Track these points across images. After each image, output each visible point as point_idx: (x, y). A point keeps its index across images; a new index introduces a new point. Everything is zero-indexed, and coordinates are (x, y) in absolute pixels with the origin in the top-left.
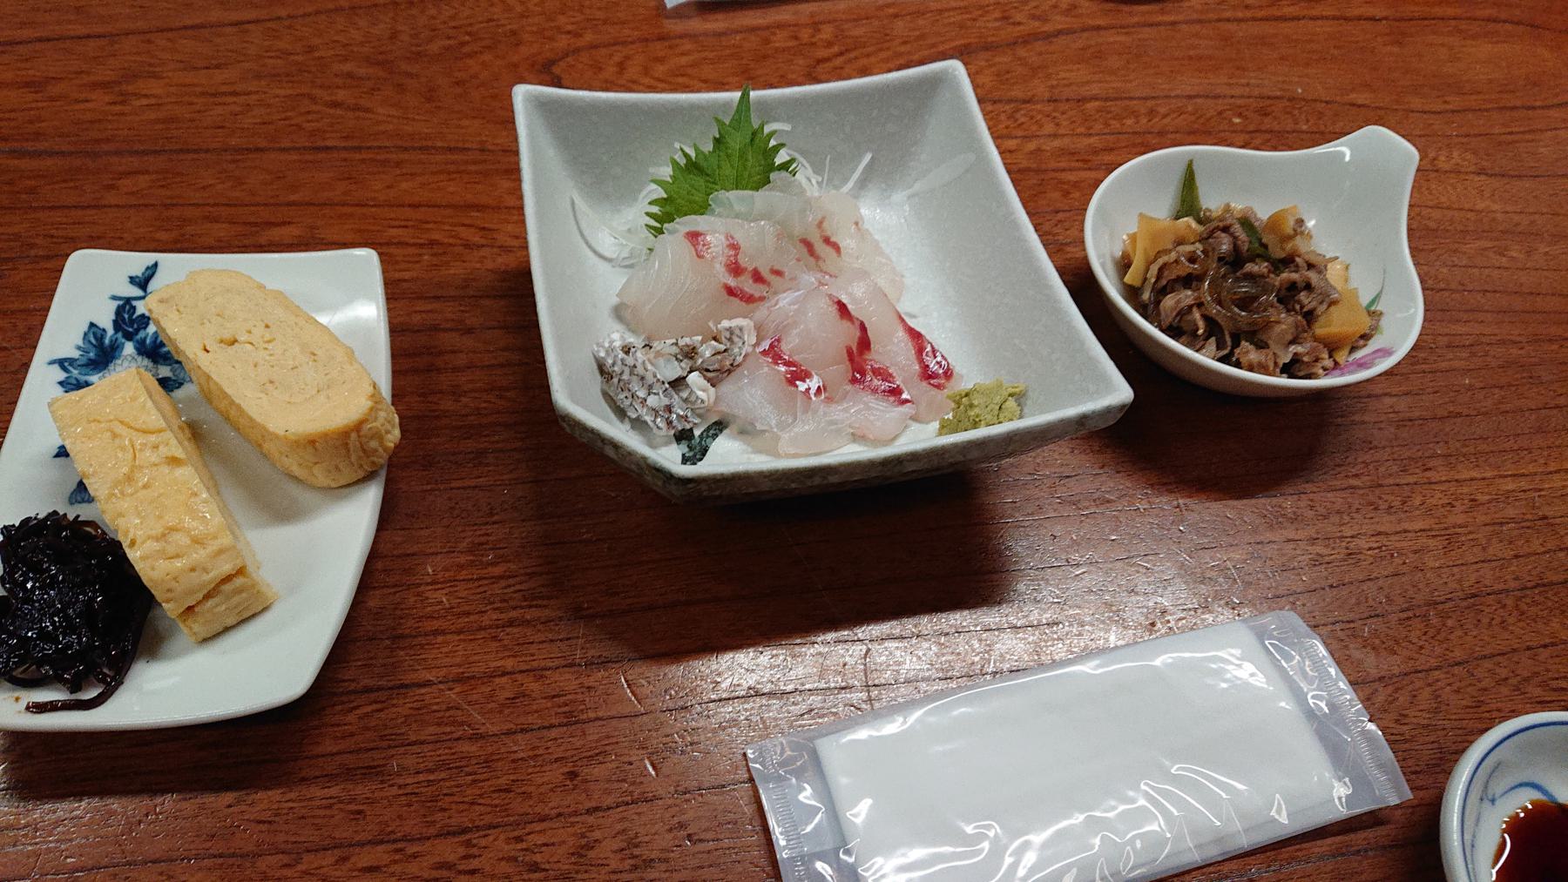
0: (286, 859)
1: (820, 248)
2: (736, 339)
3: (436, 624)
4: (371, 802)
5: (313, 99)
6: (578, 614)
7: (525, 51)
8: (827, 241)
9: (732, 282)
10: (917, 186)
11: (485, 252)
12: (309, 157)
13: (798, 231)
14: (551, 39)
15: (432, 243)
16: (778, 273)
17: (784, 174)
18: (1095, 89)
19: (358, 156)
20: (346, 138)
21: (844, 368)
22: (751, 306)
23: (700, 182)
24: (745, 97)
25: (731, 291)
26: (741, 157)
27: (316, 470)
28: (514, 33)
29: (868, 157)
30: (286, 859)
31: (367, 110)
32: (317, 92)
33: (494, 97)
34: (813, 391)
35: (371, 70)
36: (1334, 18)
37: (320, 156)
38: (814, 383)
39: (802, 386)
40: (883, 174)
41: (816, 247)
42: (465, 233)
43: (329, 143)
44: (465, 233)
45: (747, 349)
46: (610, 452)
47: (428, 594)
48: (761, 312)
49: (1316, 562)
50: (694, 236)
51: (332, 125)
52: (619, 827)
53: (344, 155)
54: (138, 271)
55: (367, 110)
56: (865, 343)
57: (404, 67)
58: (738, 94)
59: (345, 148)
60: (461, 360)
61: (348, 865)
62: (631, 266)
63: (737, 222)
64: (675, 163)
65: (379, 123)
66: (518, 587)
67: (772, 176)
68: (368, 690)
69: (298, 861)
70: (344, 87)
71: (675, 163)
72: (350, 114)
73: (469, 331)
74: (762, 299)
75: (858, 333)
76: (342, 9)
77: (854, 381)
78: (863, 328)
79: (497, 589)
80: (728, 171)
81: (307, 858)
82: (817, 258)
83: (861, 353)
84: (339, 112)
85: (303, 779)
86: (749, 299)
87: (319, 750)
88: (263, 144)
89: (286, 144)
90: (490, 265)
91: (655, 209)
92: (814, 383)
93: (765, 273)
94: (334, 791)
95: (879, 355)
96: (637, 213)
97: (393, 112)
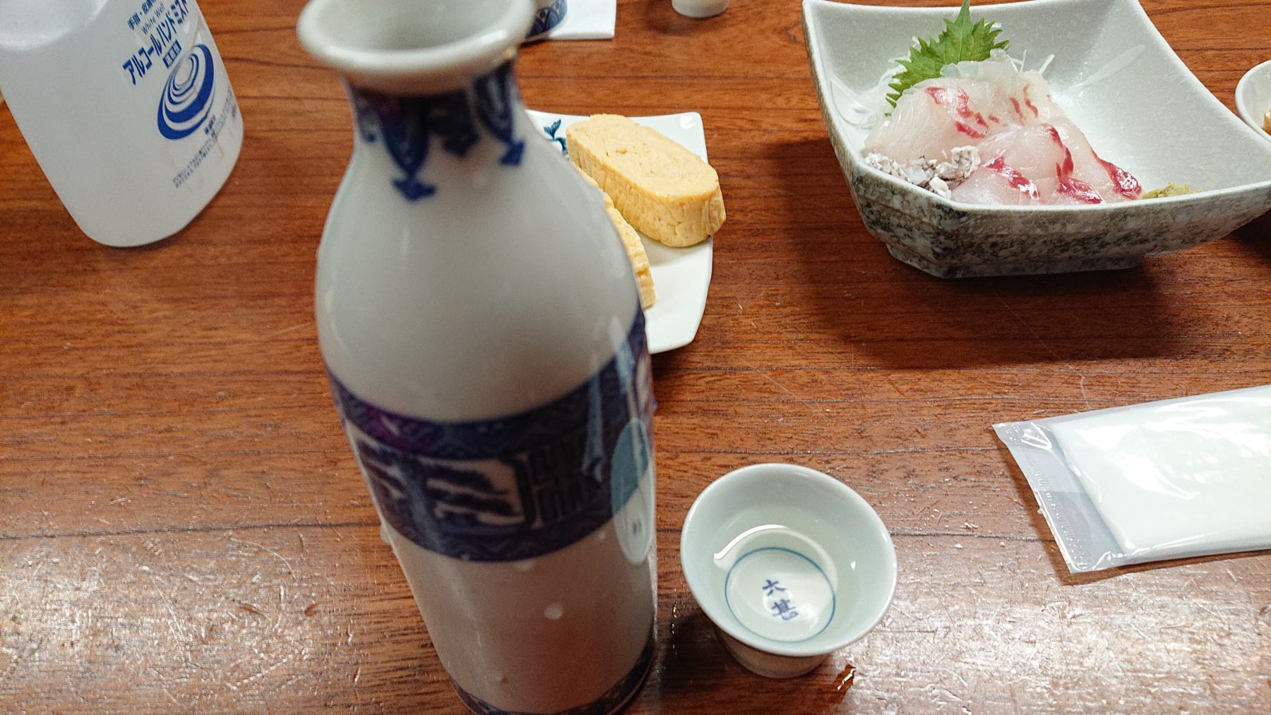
0: (668, 455)
1: (1023, 107)
2: (964, 161)
3: (749, 337)
4: (721, 429)
5: (631, 50)
6: (847, 339)
7: (767, 22)
8: (1028, 103)
9: (962, 120)
10: (1091, 79)
11: (753, 133)
13: (1009, 92)
14: (786, 15)
15: (718, 128)
16: (995, 119)
17: (1000, 51)
18: (1210, 44)
21: (1051, 181)
22: (976, 140)
23: (932, 62)
24: (965, 13)
25: (961, 128)
26: (964, 43)
27: (679, 229)
28: (760, 13)
29: (1052, 57)
30: (668, 455)
32: (635, 47)
34: (1031, 193)
38: (1032, 188)
39: (1023, 188)
40: (1062, 71)
41: (1020, 107)
42: (739, 123)
43: (646, 74)
44: (739, 123)
45: (973, 167)
46: (896, 203)
48: (984, 144)
50: (933, 91)
52: (900, 464)
54: (550, 125)
56: (1069, 165)
58: (959, 9)
60: (746, 193)
61: (709, 463)
62: (870, 128)
63: (961, 84)
64: (914, 51)
67: (992, 52)
68: (709, 369)
69: (677, 457)
71: (914, 51)
73: (748, 177)
74: (982, 136)
75: (1065, 156)
77: (1061, 190)
78: (1068, 153)
79: (788, 320)
80: (952, 53)
81: (682, 455)
82: (1021, 115)
83: (1066, 172)
84: (649, 58)
85: (674, 412)
86: (975, 135)
87: (681, 398)
88: (602, 73)
89: (617, 74)
90: (757, 140)
91: (897, 81)
92: (1032, 188)
93: (985, 119)
94: (695, 421)
95: (1078, 174)
96: (881, 91)
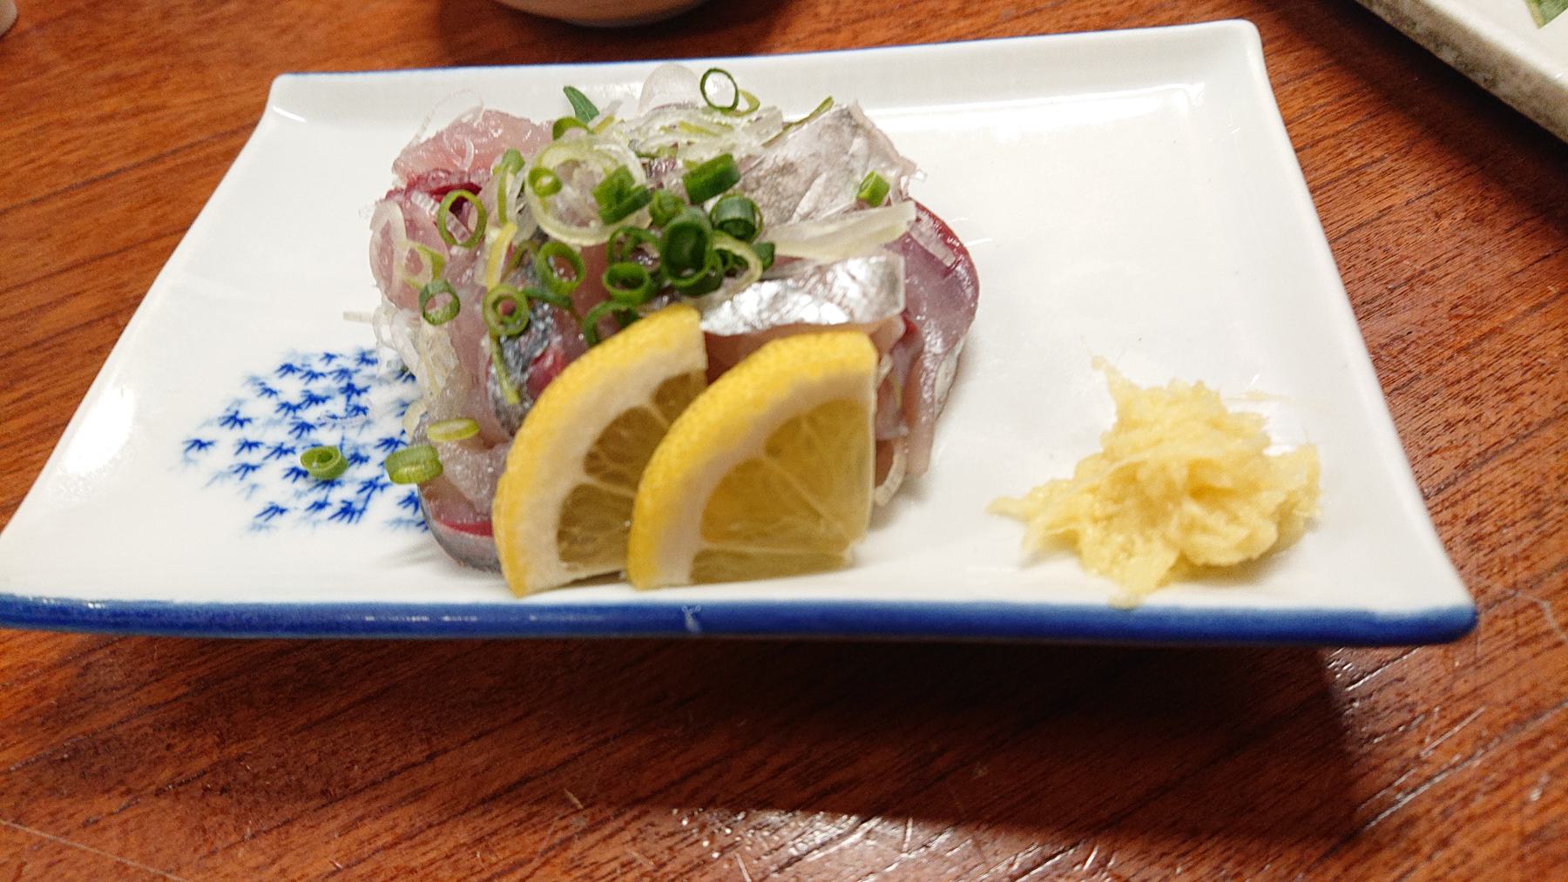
5: (67, 124)
12: (82, 196)
19: (160, 168)
20: (137, 151)
31: (156, 109)
33: (1482, 591)
35: (144, 63)
36: (84, 184)
37: (99, 189)
43: (112, 167)
47: (597, 855)
49: (1318, 83)
51: (106, 145)
53: (134, 175)
55: (156, 109)
57: (195, 41)
59: (139, 165)
65: (180, 117)
66: (776, 762)
70: (111, 94)
72: (134, 123)
76: (78, 11)
84: (112, 125)
97: (197, 96)
